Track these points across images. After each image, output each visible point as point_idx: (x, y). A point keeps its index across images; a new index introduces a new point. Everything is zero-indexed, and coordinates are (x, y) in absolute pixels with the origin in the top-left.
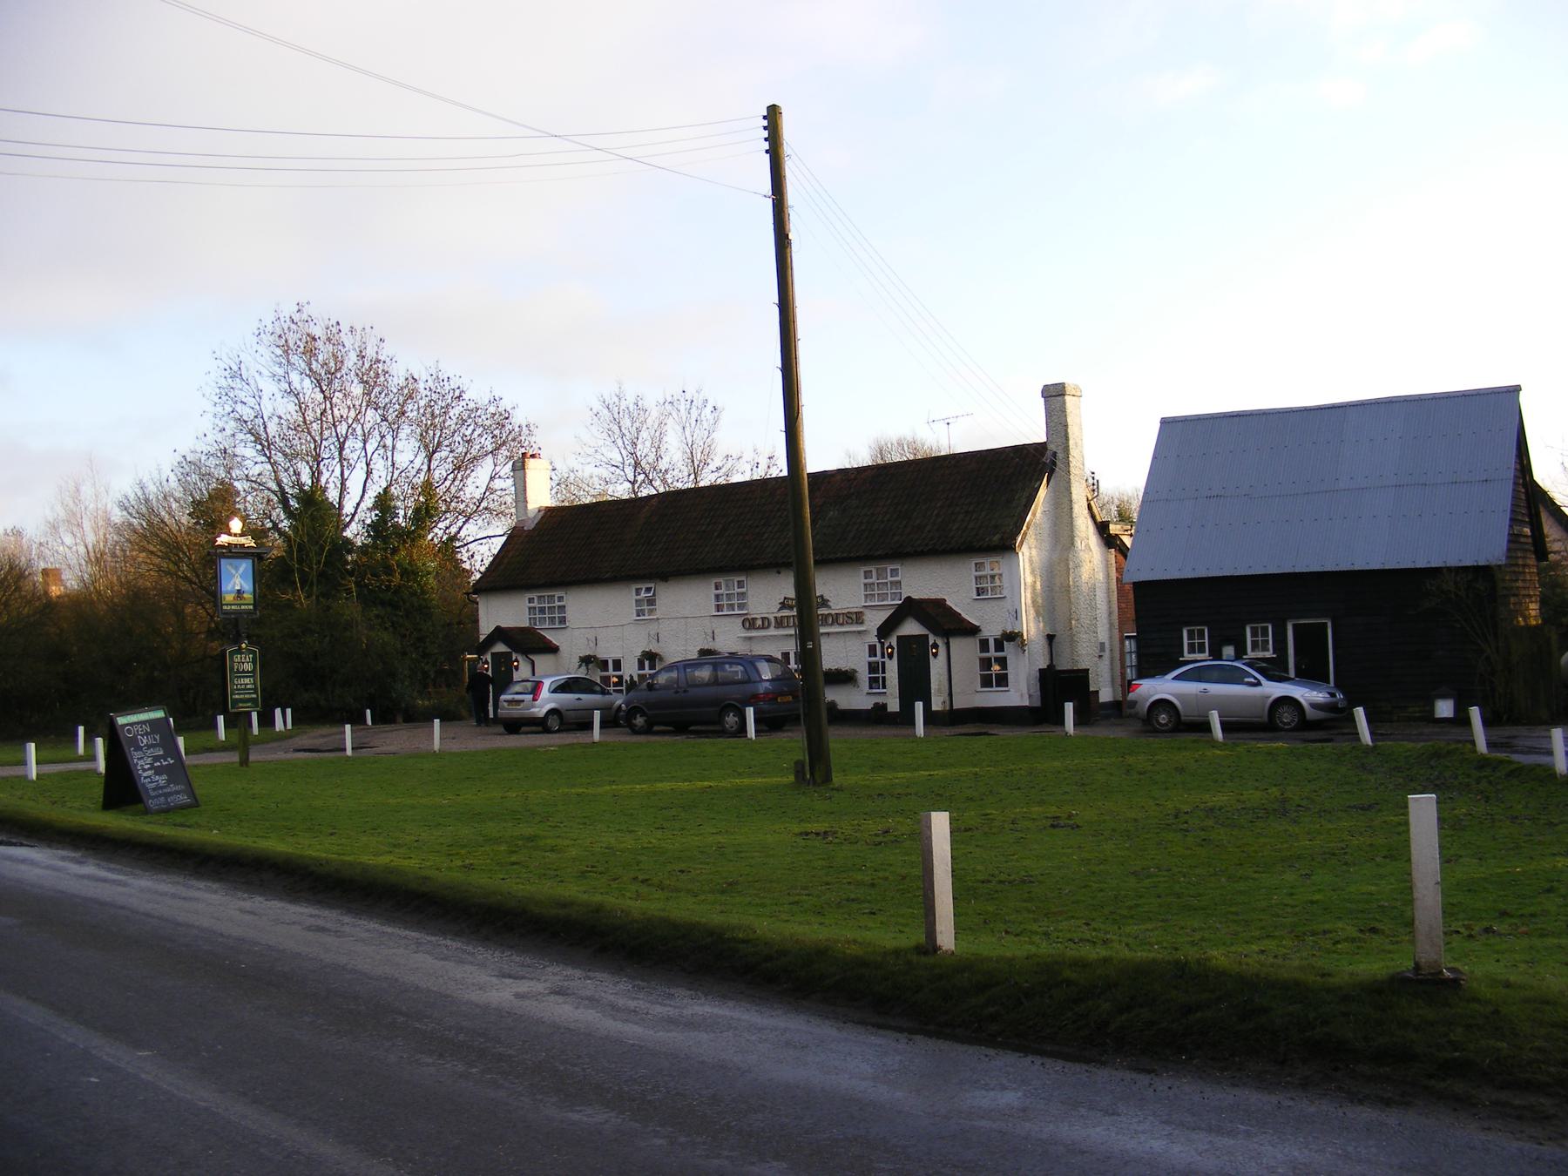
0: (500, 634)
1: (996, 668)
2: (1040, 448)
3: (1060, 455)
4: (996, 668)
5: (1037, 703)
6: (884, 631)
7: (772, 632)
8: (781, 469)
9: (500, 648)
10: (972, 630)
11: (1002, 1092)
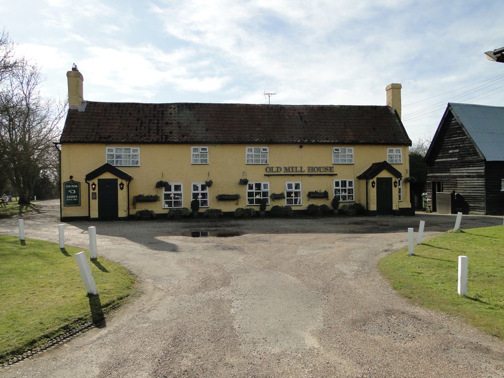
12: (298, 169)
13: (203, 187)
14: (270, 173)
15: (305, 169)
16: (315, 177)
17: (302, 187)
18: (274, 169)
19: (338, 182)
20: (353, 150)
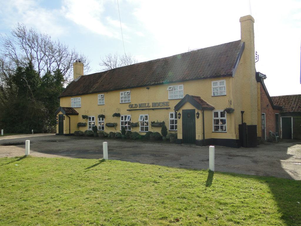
1: (220, 123)
4: (220, 123)
5: (238, 139)
10: (212, 109)
12: (147, 105)
13: (222, 115)
14: (132, 108)
15: (151, 105)
16: (159, 110)
17: (149, 119)
18: (134, 106)
19: (123, 117)
20: (183, 87)
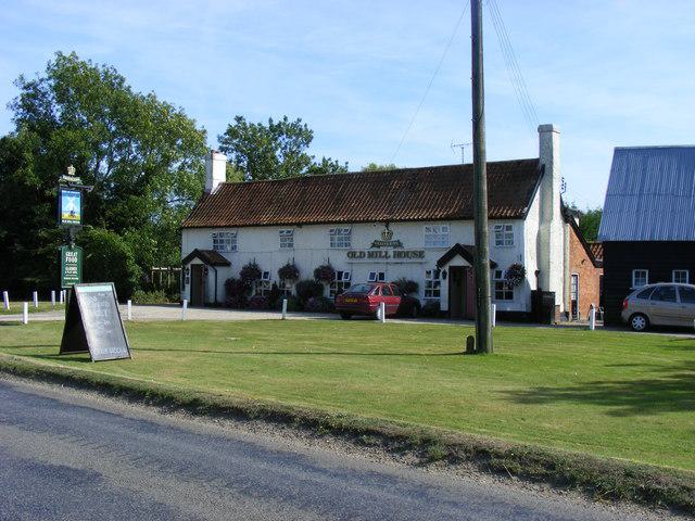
0: (197, 253)
2: (536, 161)
3: (547, 166)
6: (442, 262)
7: (366, 260)
8: (469, 160)
9: (197, 261)
11: (513, 491)
